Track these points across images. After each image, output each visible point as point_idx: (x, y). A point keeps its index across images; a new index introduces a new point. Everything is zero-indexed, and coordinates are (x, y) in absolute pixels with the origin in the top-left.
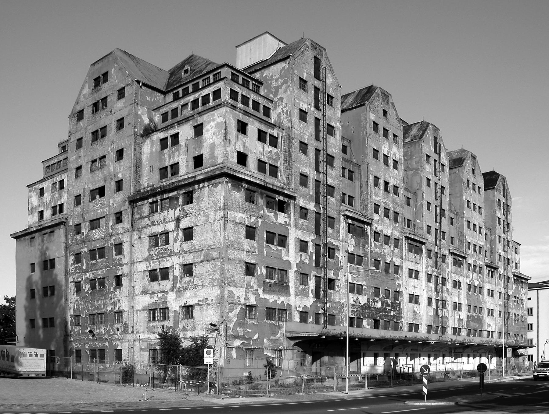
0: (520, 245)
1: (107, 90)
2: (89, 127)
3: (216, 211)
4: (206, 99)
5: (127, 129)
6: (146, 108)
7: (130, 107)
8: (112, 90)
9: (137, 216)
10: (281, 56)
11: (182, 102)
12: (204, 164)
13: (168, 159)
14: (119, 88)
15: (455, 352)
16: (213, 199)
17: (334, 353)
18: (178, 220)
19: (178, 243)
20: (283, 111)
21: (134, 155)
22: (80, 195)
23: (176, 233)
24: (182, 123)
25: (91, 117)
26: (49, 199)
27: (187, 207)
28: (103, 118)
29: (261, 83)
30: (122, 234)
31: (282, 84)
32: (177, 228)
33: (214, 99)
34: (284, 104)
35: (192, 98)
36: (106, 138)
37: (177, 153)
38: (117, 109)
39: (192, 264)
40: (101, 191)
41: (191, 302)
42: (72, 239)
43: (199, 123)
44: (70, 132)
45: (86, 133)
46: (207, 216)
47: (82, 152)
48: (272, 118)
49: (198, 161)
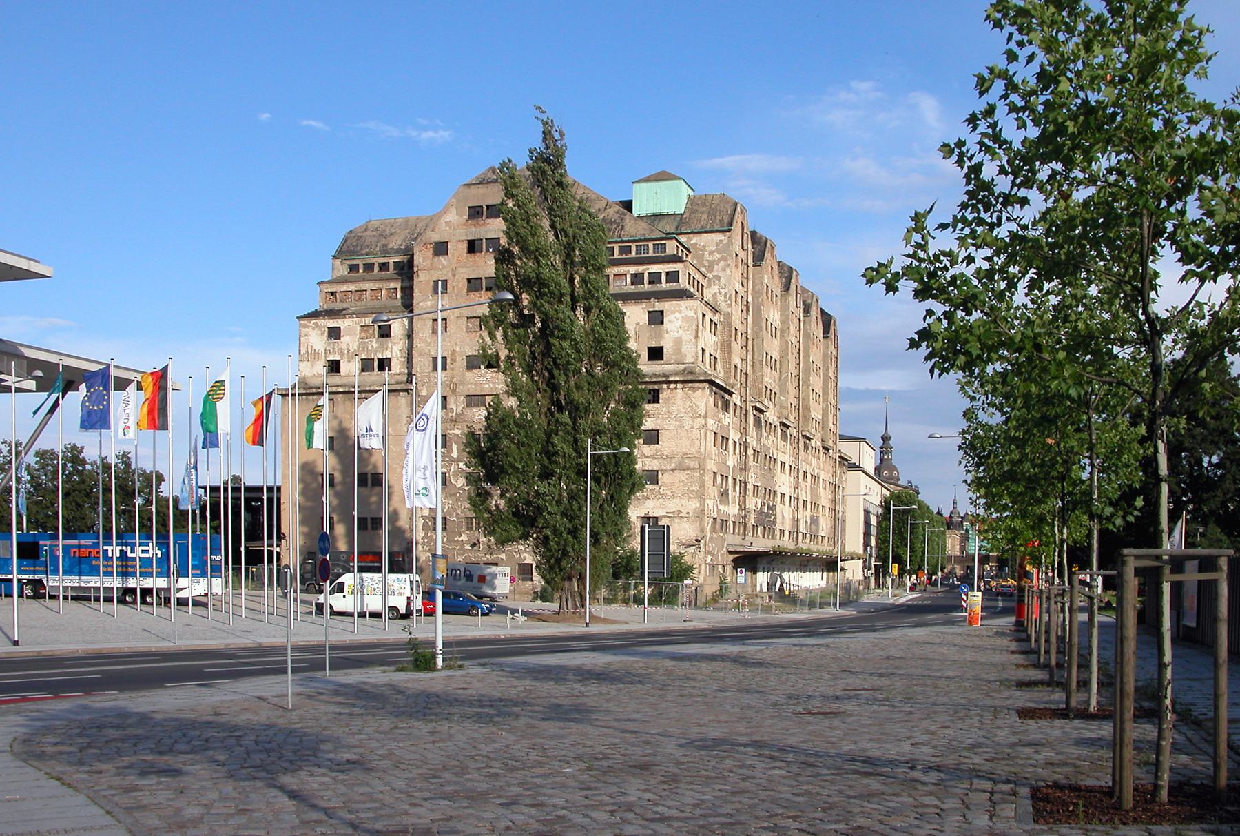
3: (694, 418)
16: (689, 404)
20: (720, 293)
31: (720, 260)
34: (722, 285)
46: (681, 421)
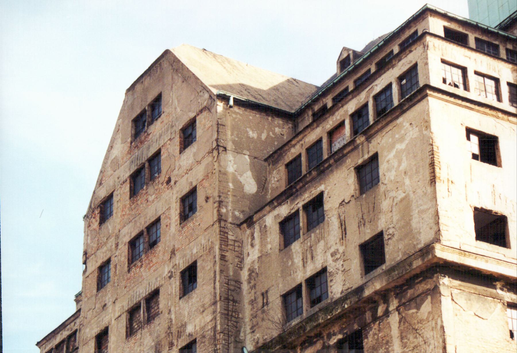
1: (160, 136)
6: (247, 157)
8: (169, 132)
11: (330, 123)
12: (387, 257)
13: (300, 264)
14: (183, 124)
21: (221, 271)
24: (328, 168)
25: (128, 206)
28: (153, 201)
35: (351, 106)
36: (160, 247)
38: (182, 171)
44: (85, 253)
45: (117, 245)
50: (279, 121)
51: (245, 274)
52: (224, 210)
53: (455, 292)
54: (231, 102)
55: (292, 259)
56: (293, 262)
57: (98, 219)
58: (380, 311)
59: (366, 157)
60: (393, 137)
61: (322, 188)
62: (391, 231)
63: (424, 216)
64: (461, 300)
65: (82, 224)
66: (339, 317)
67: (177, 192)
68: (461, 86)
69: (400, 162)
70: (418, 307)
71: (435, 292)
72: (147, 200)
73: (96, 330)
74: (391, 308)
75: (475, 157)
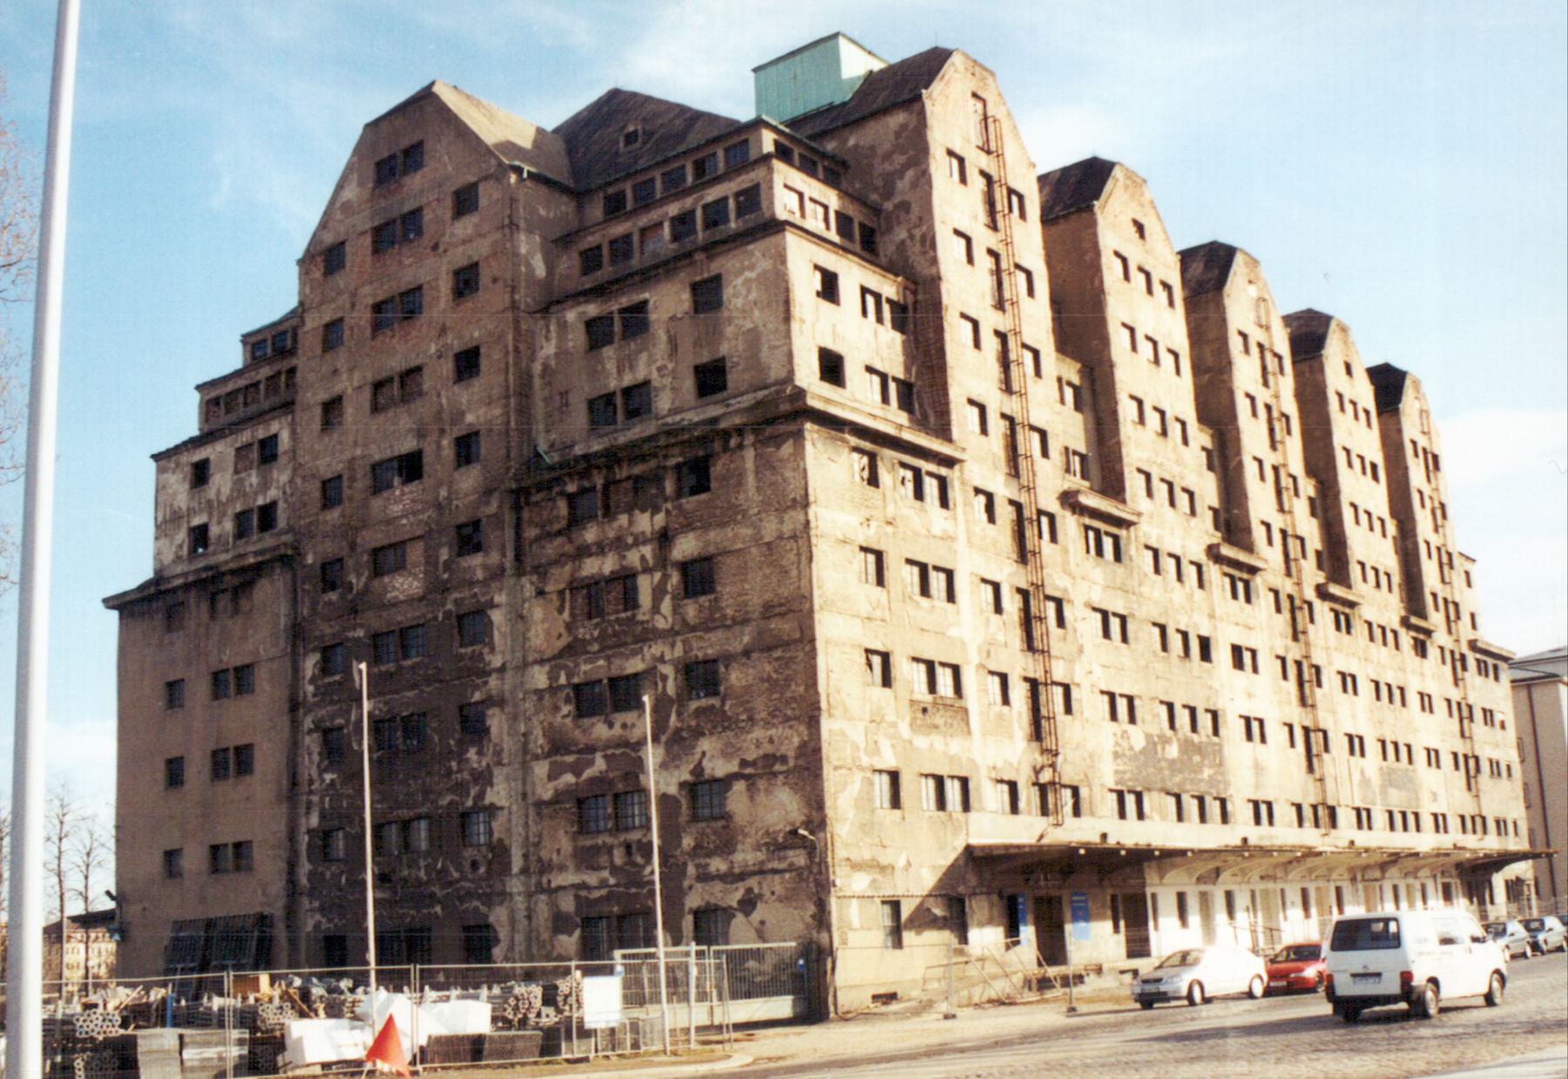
0: (1474, 561)
1: (422, 191)
2: (366, 290)
4: (715, 214)
5: (491, 297)
7: (498, 235)
9: (531, 533)
10: (885, 93)
15: (1363, 880)
17: (1083, 898)
18: (664, 538)
19: (666, 605)
20: (911, 237)
22: (339, 477)
23: (658, 576)
26: (226, 491)
27: (690, 503)
28: (410, 266)
29: (844, 164)
30: (485, 583)
32: (662, 561)
33: (740, 213)
37: (644, 356)
39: (715, 661)
40: (411, 466)
41: (719, 767)
42: (314, 604)
43: (712, 274)
45: (353, 305)
47: (341, 358)
48: (882, 254)
49: (711, 379)
50: (565, 199)
51: (537, 368)
52: (517, 297)
53: (816, 436)
54: (525, 175)
55: (602, 363)
56: (604, 367)
57: (321, 266)
58: (733, 442)
59: (706, 275)
60: (742, 262)
61: (646, 295)
62: (735, 359)
63: (775, 352)
64: (819, 445)
65: (294, 271)
66: (683, 442)
67: (449, 262)
68: (798, 214)
69: (749, 291)
70: (778, 447)
71: (799, 436)
72: (400, 262)
73: (324, 396)
74: (746, 442)
75: (433, 84)
